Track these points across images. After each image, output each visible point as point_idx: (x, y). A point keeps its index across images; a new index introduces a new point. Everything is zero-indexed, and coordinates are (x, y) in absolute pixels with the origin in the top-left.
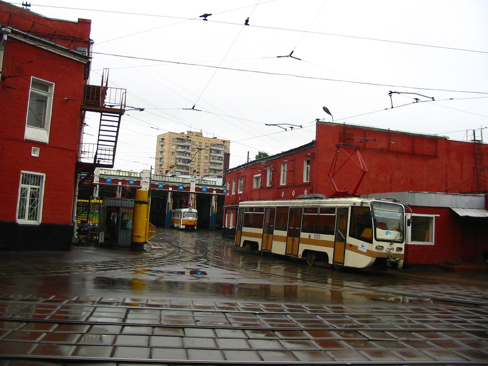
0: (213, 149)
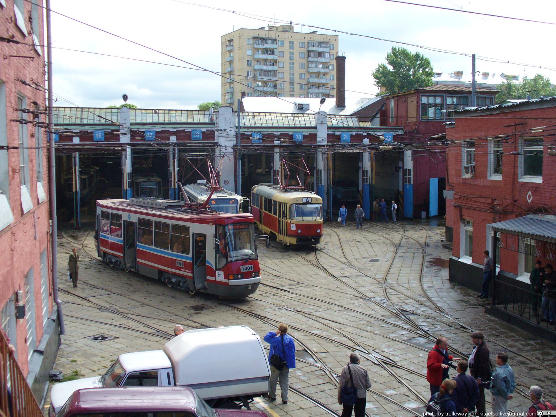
0: (312, 51)
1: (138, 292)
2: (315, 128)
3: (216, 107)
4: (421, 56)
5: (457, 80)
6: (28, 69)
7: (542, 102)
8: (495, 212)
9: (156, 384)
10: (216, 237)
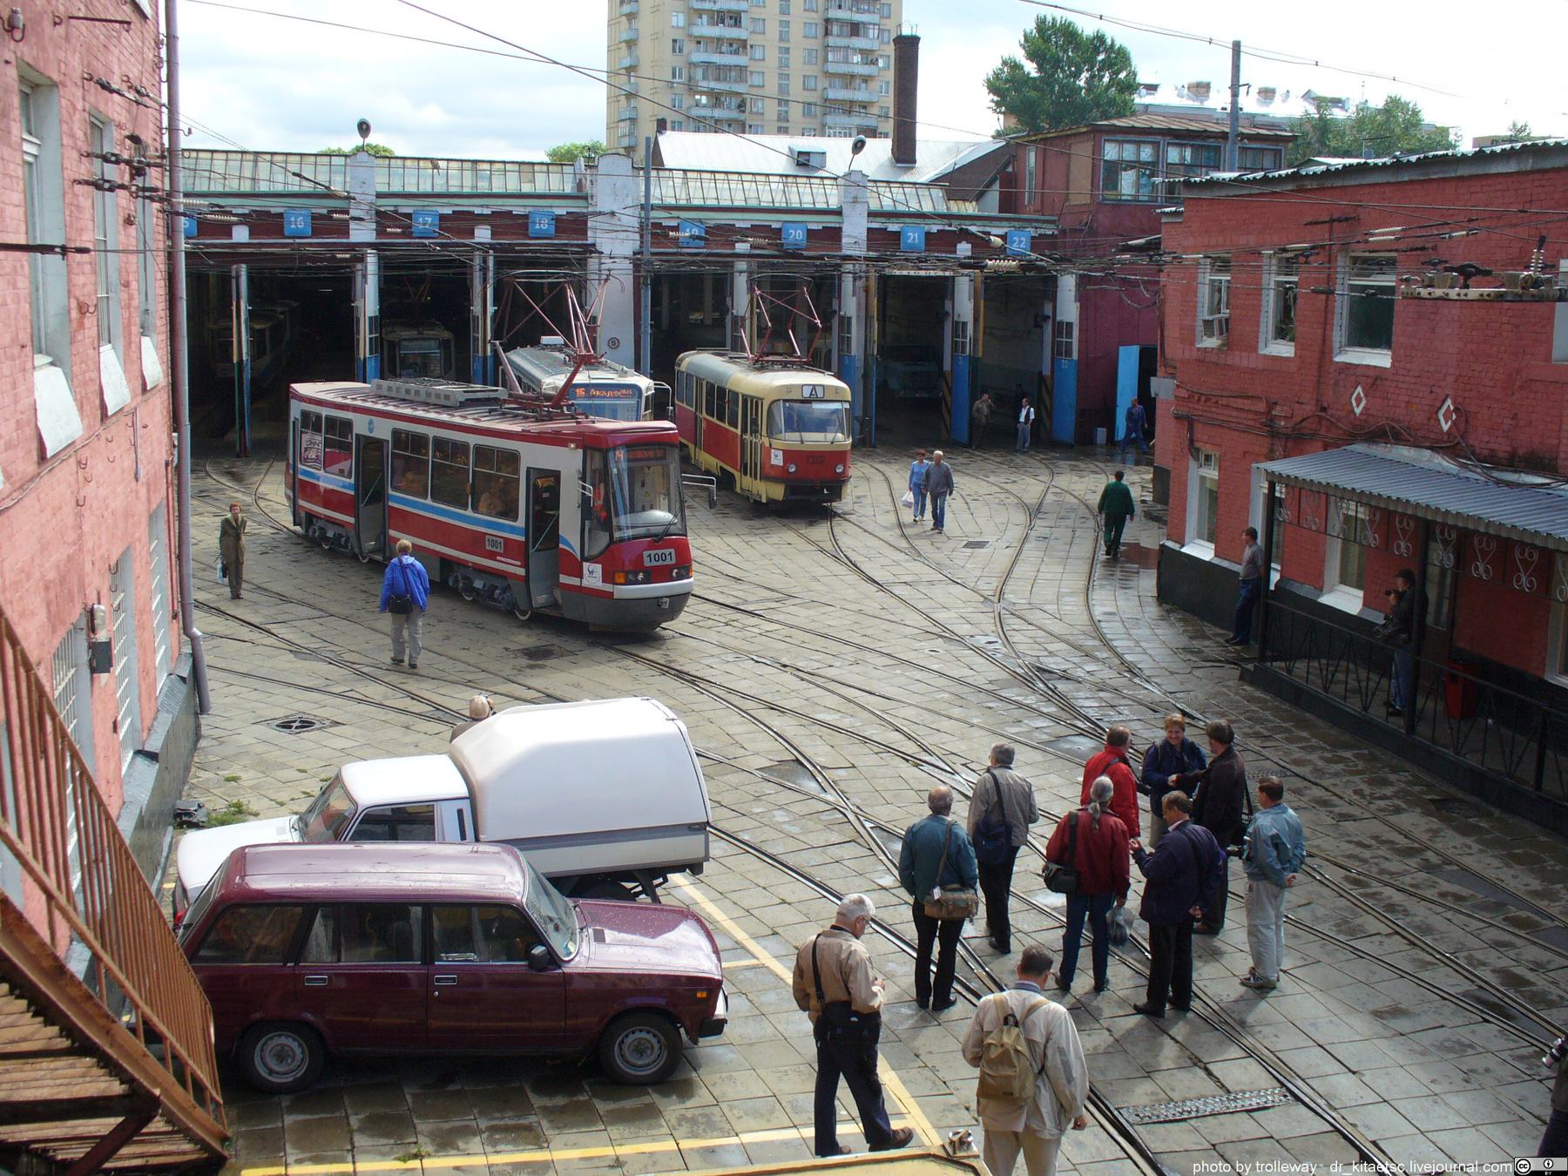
2: (838, 213)
3: (592, 156)
4: (1109, 42)
5: (1197, 104)
6: (116, 52)
7: (1398, 166)
8: (1274, 434)
9: (429, 837)
10: (583, 479)
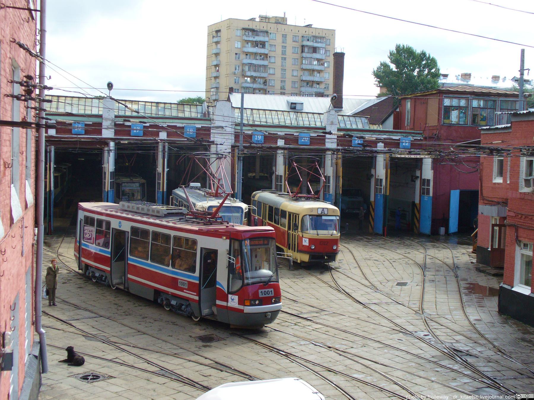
0: (307, 46)
1: (130, 315)
4: (428, 56)
5: (465, 83)
